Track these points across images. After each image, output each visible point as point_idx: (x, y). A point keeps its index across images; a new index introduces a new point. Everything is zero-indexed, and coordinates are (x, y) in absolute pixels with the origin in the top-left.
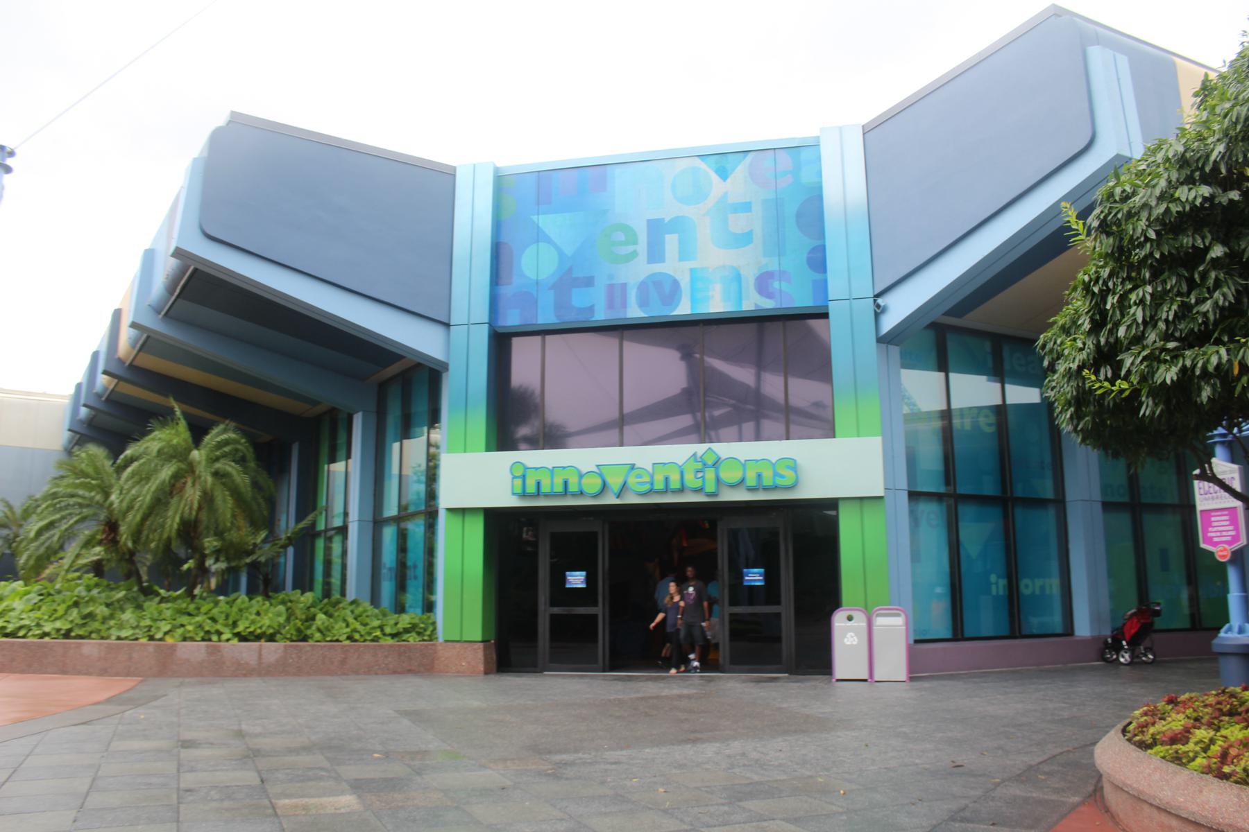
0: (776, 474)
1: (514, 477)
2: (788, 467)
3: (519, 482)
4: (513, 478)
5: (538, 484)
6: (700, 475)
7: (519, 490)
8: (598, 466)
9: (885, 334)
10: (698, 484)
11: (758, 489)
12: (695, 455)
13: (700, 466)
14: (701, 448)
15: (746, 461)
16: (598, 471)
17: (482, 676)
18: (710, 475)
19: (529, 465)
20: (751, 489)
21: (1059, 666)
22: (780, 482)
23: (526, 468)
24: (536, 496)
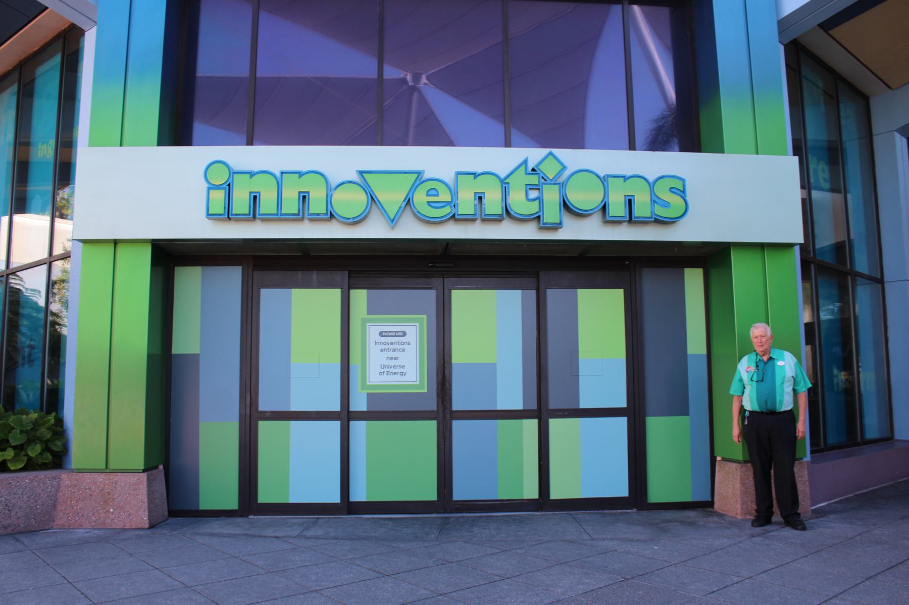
0: (655, 200)
1: (212, 187)
2: (672, 190)
3: (219, 196)
4: (209, 189)
5: (630, 203)
6: (534, 194)
7: (218, 207)
8: (361, 173)
9: (786, 17)
10: (533, 208)
11: (473, 220)
12: (525, 162)
13: (534, 180)
14: (535, 154)
15: (282, 173)
16: (451, 184)
17: (749, 530)
18: (551, 196)
19: (236, 166)
20: (611, 222)
21: (772, 472)
22: (661, 212)
23: (233, 173)
24: (248, 220)
